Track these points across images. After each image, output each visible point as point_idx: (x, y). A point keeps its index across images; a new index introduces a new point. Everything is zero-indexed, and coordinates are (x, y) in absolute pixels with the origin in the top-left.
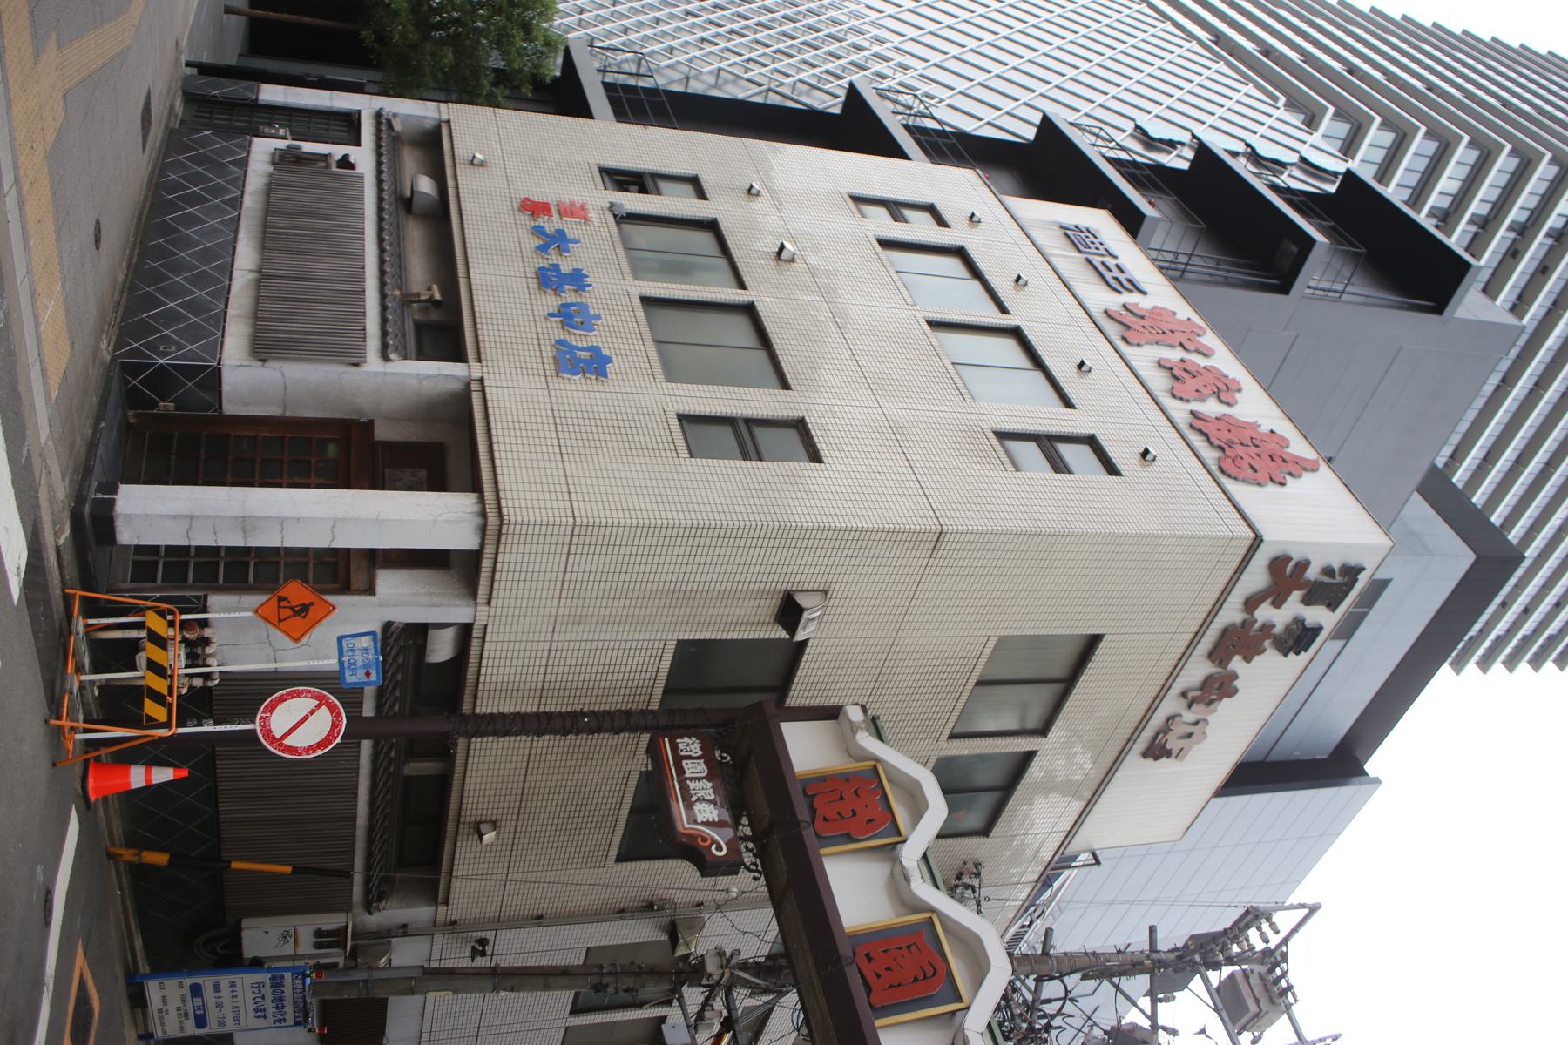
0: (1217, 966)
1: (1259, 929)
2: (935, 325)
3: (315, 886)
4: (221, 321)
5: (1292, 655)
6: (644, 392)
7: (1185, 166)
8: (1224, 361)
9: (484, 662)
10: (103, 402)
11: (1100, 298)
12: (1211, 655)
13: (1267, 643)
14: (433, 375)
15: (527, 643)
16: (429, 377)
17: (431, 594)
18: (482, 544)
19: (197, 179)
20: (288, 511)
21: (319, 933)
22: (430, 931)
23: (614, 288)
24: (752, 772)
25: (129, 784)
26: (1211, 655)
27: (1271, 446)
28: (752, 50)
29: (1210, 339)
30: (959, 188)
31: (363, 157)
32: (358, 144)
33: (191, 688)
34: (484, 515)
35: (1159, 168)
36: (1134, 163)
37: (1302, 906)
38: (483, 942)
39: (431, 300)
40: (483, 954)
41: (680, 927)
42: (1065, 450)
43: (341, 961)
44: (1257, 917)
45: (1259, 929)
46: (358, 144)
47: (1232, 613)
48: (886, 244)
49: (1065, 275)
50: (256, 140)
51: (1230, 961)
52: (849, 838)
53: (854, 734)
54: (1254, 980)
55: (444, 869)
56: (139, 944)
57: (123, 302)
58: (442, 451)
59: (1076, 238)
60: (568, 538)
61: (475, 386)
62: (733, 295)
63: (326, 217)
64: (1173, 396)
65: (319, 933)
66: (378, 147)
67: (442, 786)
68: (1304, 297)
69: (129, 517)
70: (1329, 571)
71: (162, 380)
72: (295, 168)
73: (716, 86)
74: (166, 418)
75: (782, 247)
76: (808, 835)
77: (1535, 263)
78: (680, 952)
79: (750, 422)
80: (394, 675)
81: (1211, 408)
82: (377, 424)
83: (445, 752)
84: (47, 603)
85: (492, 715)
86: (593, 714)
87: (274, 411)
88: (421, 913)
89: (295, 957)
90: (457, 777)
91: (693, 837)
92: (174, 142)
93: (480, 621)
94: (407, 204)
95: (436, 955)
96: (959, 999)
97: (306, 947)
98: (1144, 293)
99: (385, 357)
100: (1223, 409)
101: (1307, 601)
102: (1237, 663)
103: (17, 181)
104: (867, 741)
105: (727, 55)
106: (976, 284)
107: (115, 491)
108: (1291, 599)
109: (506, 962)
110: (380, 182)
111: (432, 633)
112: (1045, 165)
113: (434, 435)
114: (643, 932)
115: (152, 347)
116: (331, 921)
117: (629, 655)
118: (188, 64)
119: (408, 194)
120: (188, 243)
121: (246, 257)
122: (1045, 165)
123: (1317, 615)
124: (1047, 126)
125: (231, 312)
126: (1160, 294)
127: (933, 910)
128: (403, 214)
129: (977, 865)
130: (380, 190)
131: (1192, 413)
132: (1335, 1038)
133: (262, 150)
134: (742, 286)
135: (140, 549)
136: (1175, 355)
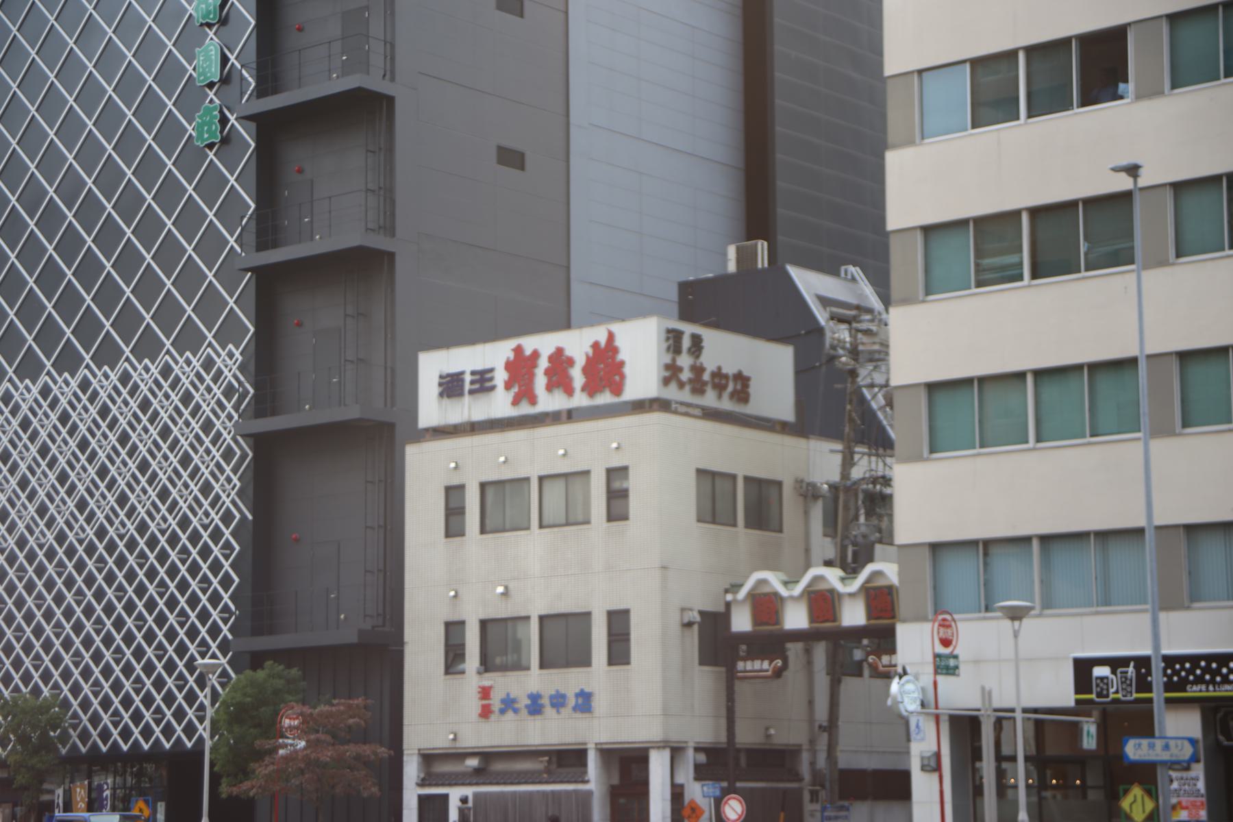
1: (808, 651)
6: (598, 674)
15: (702, 728)
21: (812, 801)
22: (814, 752)
25: (904, 621)
31: (455, 795)
38: (820, 727)
45: (808, 651)
58: (628, 765)
65: (812, 801)
83: (739, 750)
88: (805, 757)
97: (817, 807)
104: (742, 594)
116: (806, 796)
117: (705, 680)
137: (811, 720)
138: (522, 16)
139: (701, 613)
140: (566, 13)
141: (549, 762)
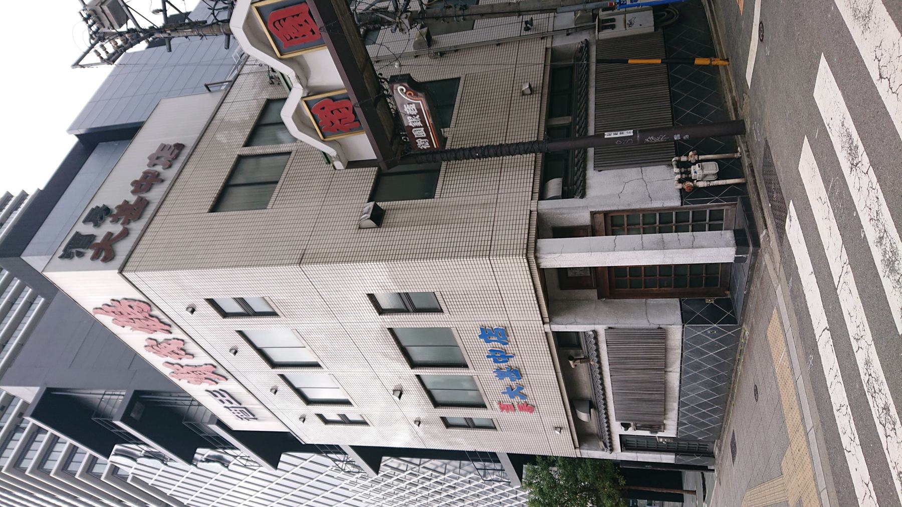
0: (129, 31)
2: (316, 365)
3: (615, 54)
5: (101, 205)
6: (461, 323)
7: (198, 450)
8: (157, 361)
10: (745, 304)
11: (230, 386)
13: (115, 212)
15: (512, 190)
18: (536, 242)
19: (704, 415)
22: (556, 32)
23: (482, 373)
27: (122, 319)
29: (166, 371)
30: (312, 432)
31: (617, 429)
33: (687, 155)
34: (536, 258)
35: (213, 448)
37: (82, 66)
40: (526, 23)
41: (426, 44)
42: (238, 309)
43: (601, 13)
44: (108, 59)
45: (107, 52)
47: (136, 227)
48: (346, 403)
49: (250, 395)
51: (121, 34)
53: (338, 155)
54: (107, 24)
55: (549, 67)
56: (708, 14)
57: (738, 355)
58: (561, 290)
59: (250, 414)
61: (547, 320)
62: (423, 372)
64: (183, 340)
65: (613, 27)
66: (610, 435)
70: (80, 255)
74: (710, 295)
75: (400, 397)
77: (8, 411)
78: (425, 30)
79: (405, 311)
80: (578, 170)
81: (161, 336)
83: (550, 131)
84: (771, 199)
87: (652, 301)
88: (560, 42)
89: (625, 13)
90: (543, 118)
92: (718, 433)
94: (592, 405)
95: (551, 20)
96: (257, 8)
97: (619, 19)
99: (595, 332)
100: (154, 336)
101: (92, 237)
102: (132, 199)
104: (331, 151)
109: (515, 19)
110: (607, 418)
112: (272, 446)
113: (566, 293)
114: (446, 40)
116: (606, 34)
117: (457, 187)
118: (713, 470)
120: (705, 384)
121: (674, 378)
122: (272, 446)
123: (88, 229)
126: (198, 391)
127: (280, 60)
128: (594, 400)
130: (606, 413)
131: (171, 333)
132: (298, 15)
133: (670, 431)
134: (418, 376)
135: (719, 228)
136: (185, 361)
137: (519, 40)
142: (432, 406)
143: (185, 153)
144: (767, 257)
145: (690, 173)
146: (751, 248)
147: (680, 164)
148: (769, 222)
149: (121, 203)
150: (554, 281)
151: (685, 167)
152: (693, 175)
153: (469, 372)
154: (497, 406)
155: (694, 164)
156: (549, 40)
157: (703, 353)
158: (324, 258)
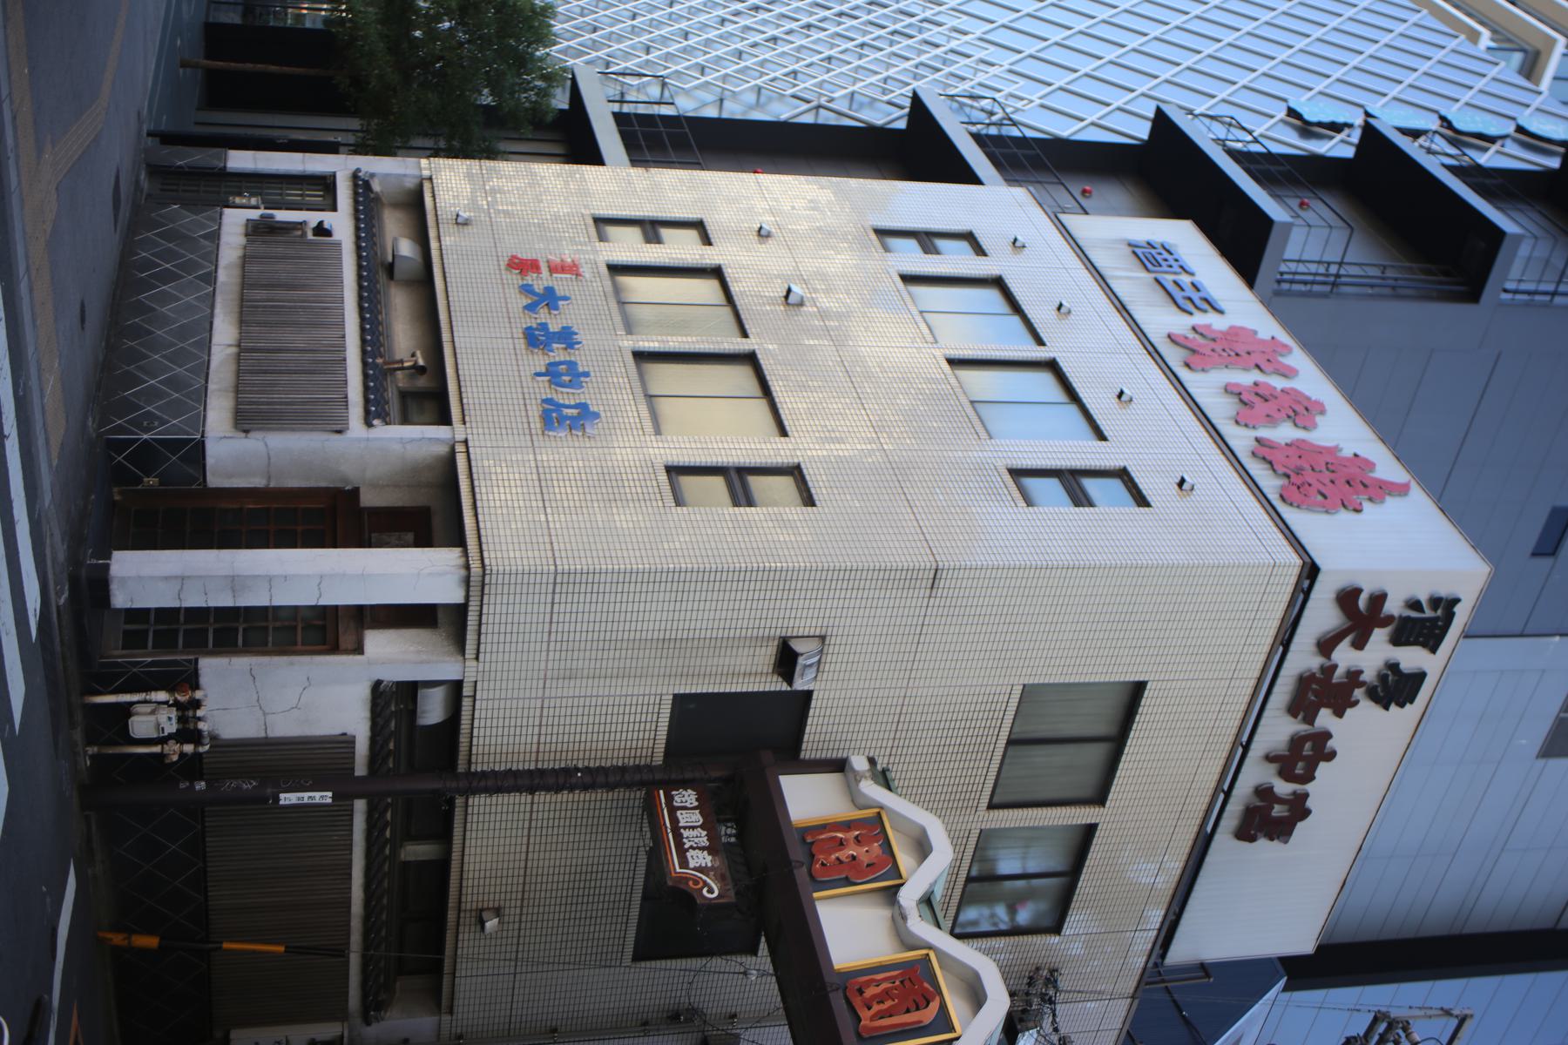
2: (954, 362)
4: (202, 395)
7: (1348, 152)
8: (1310, 380)
9: (476, 724)
11: (1161, 320)
12: (1293, 709)
14: (416, 440)
15: (519, 702)
16: (412, 440)
17: (419, 652)
18: (467, 597)
19: (169, 255)
20: (276, 570)
24: (746, 811)
26: (1293, 709)
28: (895, 21)
29: (1298, 359)
30: (998, 207)
31: (341, 223)
32: (334, 208)
34: (467, 567)
36: (1269, 157)
39: (415, 367)
42: (1090, 485)
46: (334, 208)
47: (1302, 658)
48: (909, 279)
50: (227, 211)
52: (848, 882)
53: (858, 782)
58: (431, 512)
59: (1149, 257)
60: (551, 587)
61: (460, 448)
62: (736, 344)
63: (303, 287)
67: (440, 869)
68: (1502, 304)
69: (123, 580)
70: (1415, 605)
71: (147, 455)
72: (268, 238)
73: (758, 105)
75: (789, 291)
76: (801, 874)
81: (1284, 433)
82: (362, 491)
85: (483, 772)
86: (587, 770)
87: (258, 482)
90: (455, 856)
91: (686, 879)
93: (469, 679)
96: (952, 1029)
98: (1221, 312)
100: (1299, 434)
101: (1397, 640)
102: (1325, 718)
103: (28, 269)
104: (872, 790)
105: (870, 28)
106: (1016, 319)
107: (109, 557)
108: (1373, 638)
111: (421, 693)
115: (136, 423)
117: (627, 714)
118: (149, 134)
119: (390, 259)
121: (224, 333)
123: (1411, 658)
124: (1161, 122)
125: (211, 386)
127: (930, 947)
129: (1052, 971)
131: (1257, 440)
133: (235, 221)
134: (745, 335)
136: (1246, 378)
138: (1534, 554)
139: (808, 694)
140: (1521, 635)
141: (420, 370)
142: (729, 273)
143: (1231, 820)
144: (61, 556)
145: (180, 720)
146: (83, 573)
147: (195, 737)
148: (55, 616)
149: (1349, 712)
150: (438, 523)
151: (188, 732)
152: (174, 713)
153: (629, 343)
154: (586, 271)
155: (170, 736)
156: (445, 1032)
157: (168, 382)
158: (892, 578)
